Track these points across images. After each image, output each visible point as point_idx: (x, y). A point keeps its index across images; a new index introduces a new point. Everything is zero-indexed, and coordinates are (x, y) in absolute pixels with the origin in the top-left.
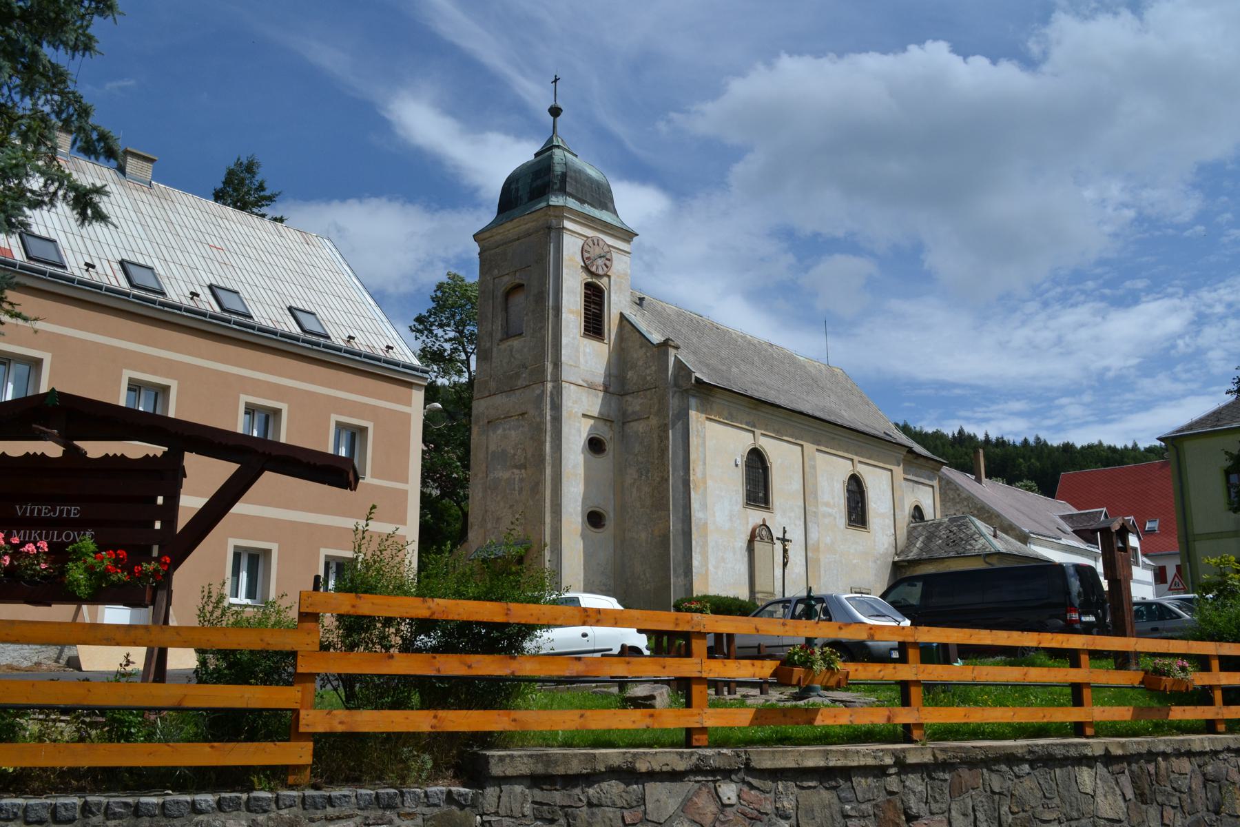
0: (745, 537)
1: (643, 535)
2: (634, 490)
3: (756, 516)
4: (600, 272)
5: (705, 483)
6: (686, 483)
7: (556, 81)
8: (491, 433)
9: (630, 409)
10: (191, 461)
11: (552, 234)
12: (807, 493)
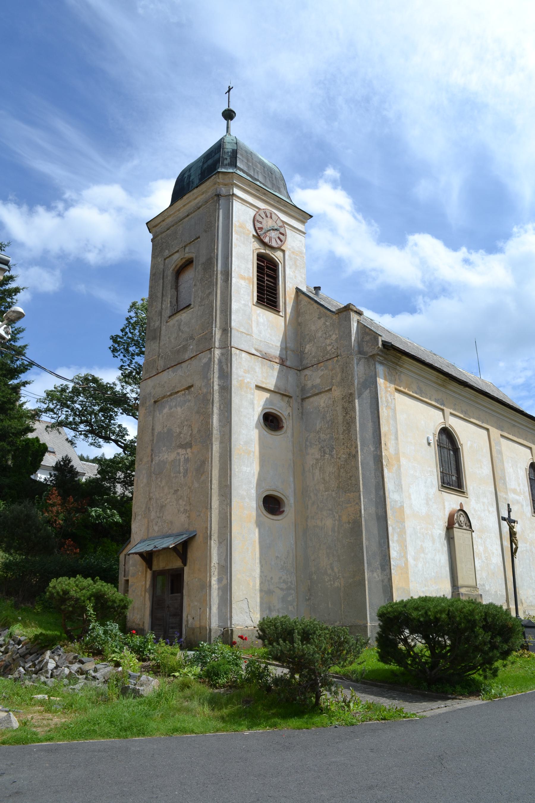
0: (443, 523)
1: (329, 523)
2: (317, 472)
3: (452, 501)
4: (274, 244)
5: (398, 460)
6: (378, 460)
7: (229, 91)
8: (157, 413)
9: (309, 384)
11: (222, 201)
12: (496, 479)
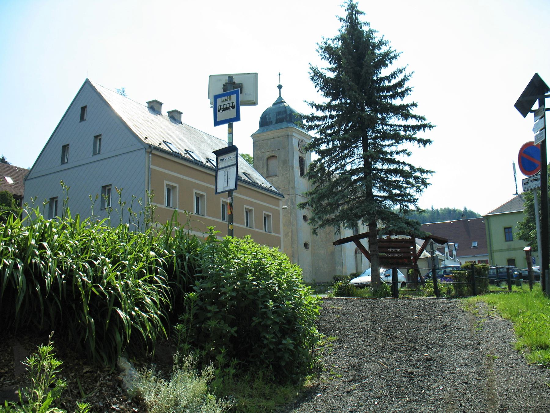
10: (417, 240)
11: (290, 138)
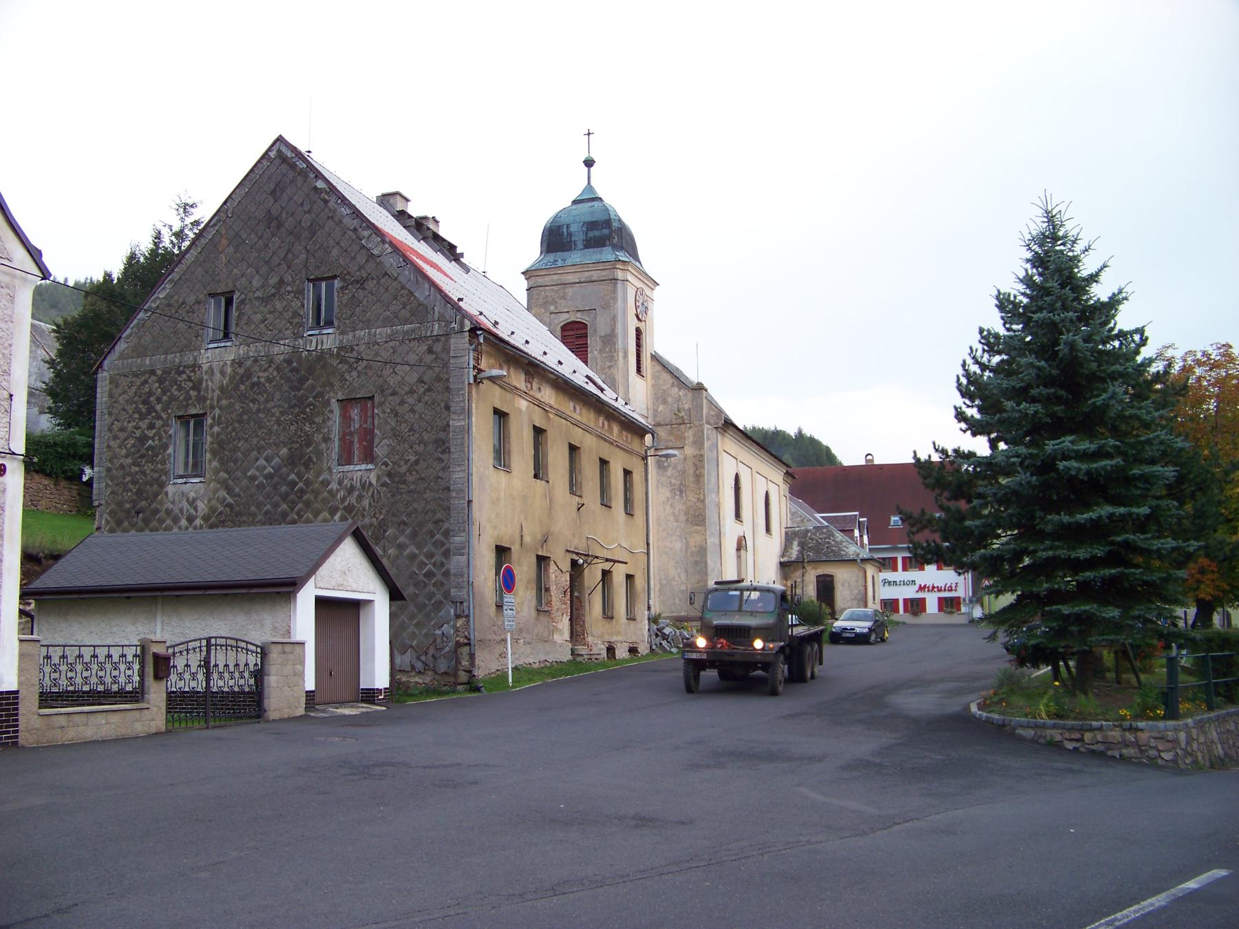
2: (668, 507)
11: (619, 285)
